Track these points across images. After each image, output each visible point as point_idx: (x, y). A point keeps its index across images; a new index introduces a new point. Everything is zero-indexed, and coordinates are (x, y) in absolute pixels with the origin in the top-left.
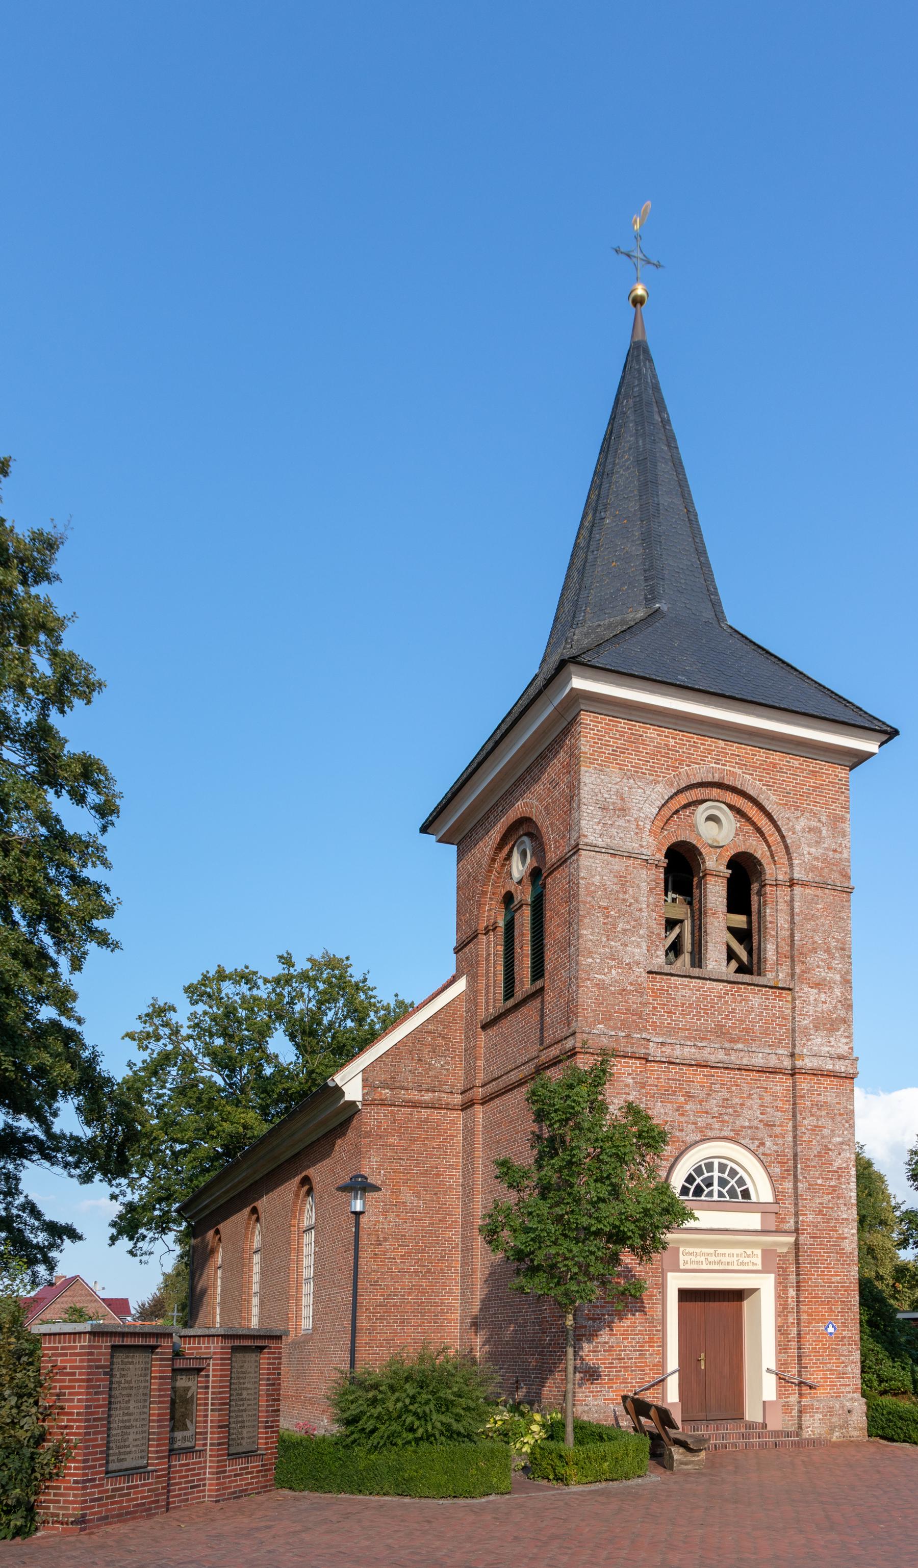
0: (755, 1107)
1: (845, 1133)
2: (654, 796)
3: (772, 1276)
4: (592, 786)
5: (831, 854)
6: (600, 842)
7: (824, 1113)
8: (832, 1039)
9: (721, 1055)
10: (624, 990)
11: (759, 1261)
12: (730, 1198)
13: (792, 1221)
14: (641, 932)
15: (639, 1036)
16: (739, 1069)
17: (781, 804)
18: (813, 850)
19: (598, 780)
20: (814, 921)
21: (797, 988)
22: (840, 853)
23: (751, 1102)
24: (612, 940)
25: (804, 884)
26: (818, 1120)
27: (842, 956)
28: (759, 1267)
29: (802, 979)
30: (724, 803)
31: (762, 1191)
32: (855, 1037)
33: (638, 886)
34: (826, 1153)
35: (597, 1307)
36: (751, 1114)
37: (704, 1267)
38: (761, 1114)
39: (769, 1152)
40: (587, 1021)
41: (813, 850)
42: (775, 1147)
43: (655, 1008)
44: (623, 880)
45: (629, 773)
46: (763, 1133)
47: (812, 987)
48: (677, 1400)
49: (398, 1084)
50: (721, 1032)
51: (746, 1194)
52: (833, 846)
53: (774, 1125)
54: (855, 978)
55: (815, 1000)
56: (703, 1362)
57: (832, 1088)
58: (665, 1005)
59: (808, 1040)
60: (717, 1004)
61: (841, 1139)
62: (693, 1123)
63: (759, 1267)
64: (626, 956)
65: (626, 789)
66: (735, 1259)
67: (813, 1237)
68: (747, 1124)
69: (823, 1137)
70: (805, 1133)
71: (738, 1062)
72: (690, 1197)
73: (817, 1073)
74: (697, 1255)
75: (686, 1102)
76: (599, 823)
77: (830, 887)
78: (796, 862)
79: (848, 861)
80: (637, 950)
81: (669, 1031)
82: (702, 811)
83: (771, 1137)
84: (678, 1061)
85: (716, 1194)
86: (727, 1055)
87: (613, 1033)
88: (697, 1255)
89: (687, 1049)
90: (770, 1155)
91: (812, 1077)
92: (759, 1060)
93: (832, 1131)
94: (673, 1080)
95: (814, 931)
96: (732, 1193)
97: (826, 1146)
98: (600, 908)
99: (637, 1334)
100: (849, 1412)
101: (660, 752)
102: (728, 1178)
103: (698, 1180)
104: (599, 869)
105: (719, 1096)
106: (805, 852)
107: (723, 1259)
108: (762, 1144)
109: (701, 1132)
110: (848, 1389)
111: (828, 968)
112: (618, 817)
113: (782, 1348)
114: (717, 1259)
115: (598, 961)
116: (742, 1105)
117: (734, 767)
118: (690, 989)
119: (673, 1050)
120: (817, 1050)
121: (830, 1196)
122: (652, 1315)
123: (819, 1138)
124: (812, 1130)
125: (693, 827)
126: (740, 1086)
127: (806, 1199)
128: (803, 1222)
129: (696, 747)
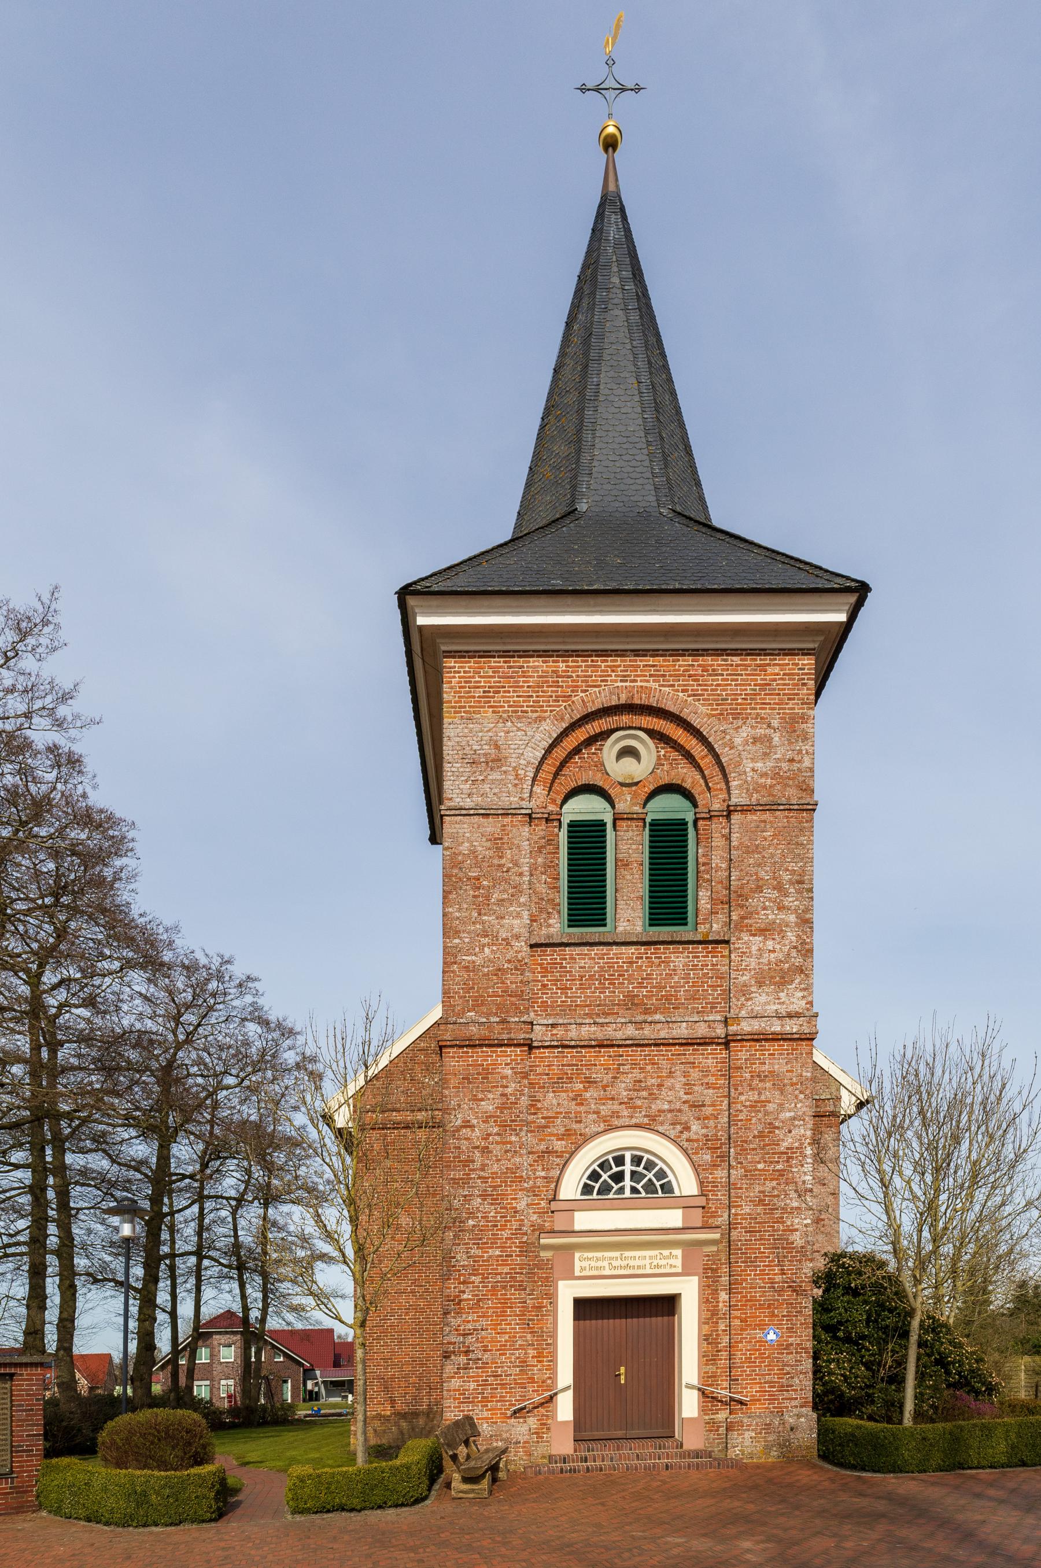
0: (678, 1086)
1: (799, 1106)
2: (538, 736)
3: (696, 1278)
4: (458, 739)
5: (785, 766)
6: (468, 803)
7: (768, 1085)
8: (782, 995)
9: (630, 1031)
10: (499, 970)
11: (678, 1263)
12: (647, 1193)
13: (726, 1215)
14: (522, 900)
15: (517, 1019)
16: (656, 1045)
17: (713, 715)
18: (759, 765)
19: (466, 731)
20: (760, 853)
21: (733, 939)
22: (799, 762)
23: (672, 1081)
24: (485, 915)
25: (746, 809)
26: (760, 1094)
27: (799, 892)
28: (680, 1270)
29: (740, 927)
30: (640, 729)
31: (686, 1183)
32: (815, 989)
33: (518, 847)
34: (770, 1132)
35: (469, 1322)
36: (674, 1094)
37: (607, 1272)
38: (686, 1094)
39: (695, 1137)
40: (453, 1011)
41: (759, 765)
42: (704, 1131)
43: (544, 986)
44: (498, 844)
45: (505, 715)
46: (688, 1115)
47: (754, 935)
48: (572, 1418)
49: (389, 1106)
50: (632, 1002)
51: (667, 1188)
52: (790, 755)
53: (704, 1106)
54: (819, 917)
55: (760, 949)
56: (622, 1377)
57: (781, 1054)
58: (558, 980)
59: (747, 1000)
60: (627, 971)
61: (792, 1114)
62: (594, 1113)
63: (680, 1270)
64: (502, 931)
65: (502, 734)
66: (647, 1262)
67: (750, 1232)
68: (666, 1107)
69: (766, 1113)
70: (741, 1111)
71: (652, 1037)
72: (595, 1196)
73: (759, 1038)
74: (598, 1259)
75: (586, 1089)
76: (467, 781)
77: (782, 807)
78: (733, 784)
79: (812, 770)
80: (516, 922)
81: (565, 1010)
82: (610, 749)
83: (699, 1119)
84: (573, 1043)
85: (628, 1190)
86: (639, 1029)
87: (484, 1020)
88: (598, 1259)
89: (585, 1029)
90: (697, 1140)
91: (753, 1044)
92: (682, 1031)
93: (781, 1105)
94: (569, 1065)
95: (759, 865)
96: (650, 1187)
97: (770, 1124)
98: (469, 879)
99: (517, 1349)
100: (792, 1429)
101: (547, 682)
102: (645, 1172)
103: (605, 1177)
104: (467, 835)
105: (629, 1079)
106: (748, 770)
107: (632, 1263)
108: (687, 1128)
109: (605, 1121)
110: (794, 1403)
111: (779, 909)
112: (492, 770)
113: (707, 1358)
114: (624, 1263)
115: (467, 940)
116: (660, 1086)
117: (648, 681)
118: (590, 959)
119: (566, 1031)
120: (762, 1007)
121: (774, 1183)
122: (541, 1328)
123: (760, 1115)
124: (751, 1106)
125: (601, 766)
126: (658, 1064)
127: (740, 1188)
128: (736, 1215)
129: (595, 666)
